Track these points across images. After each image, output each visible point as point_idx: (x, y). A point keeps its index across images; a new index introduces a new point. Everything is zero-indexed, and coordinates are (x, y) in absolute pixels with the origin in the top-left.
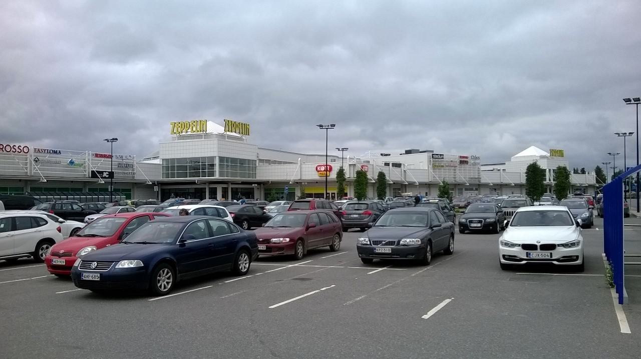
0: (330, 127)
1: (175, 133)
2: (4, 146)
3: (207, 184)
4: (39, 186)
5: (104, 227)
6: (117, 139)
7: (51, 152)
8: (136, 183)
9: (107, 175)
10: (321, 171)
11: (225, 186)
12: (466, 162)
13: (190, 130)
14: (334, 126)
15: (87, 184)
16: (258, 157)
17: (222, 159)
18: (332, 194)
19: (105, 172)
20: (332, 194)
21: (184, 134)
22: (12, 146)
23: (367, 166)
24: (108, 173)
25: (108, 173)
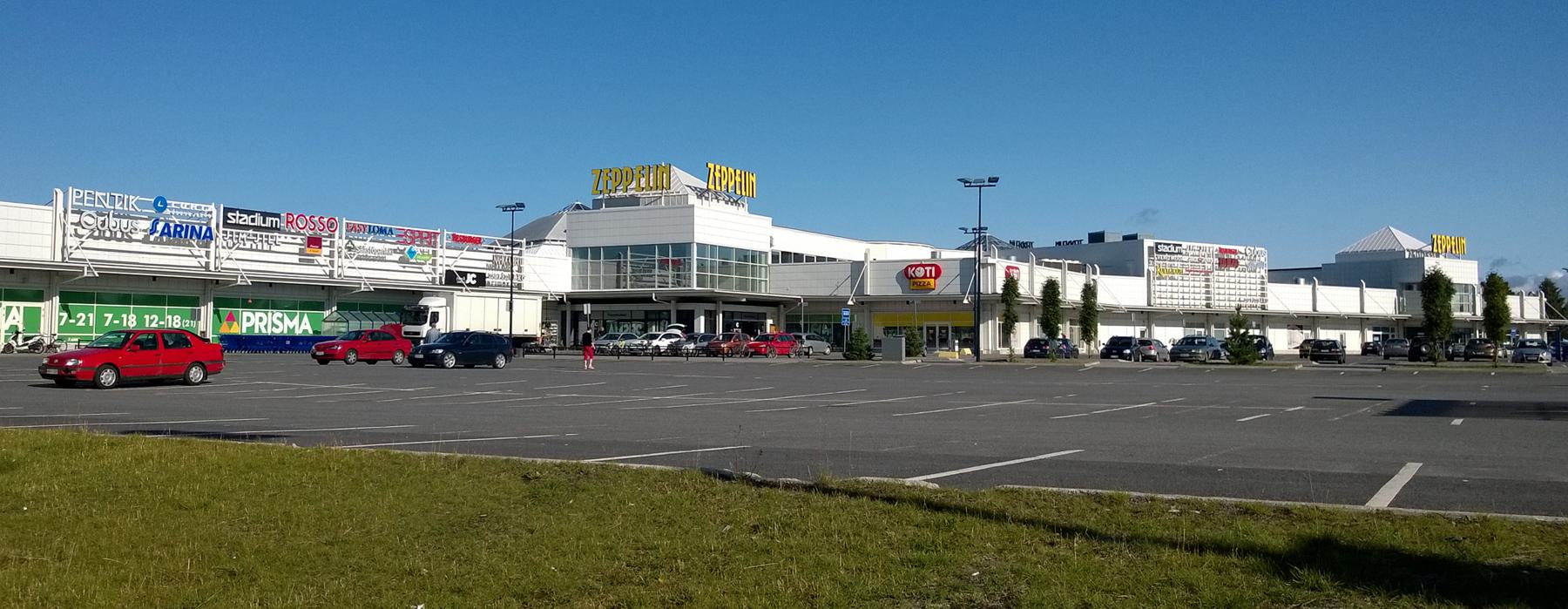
0: (986, 183)
1: (643, 188)
2: (295, 217)
3: (673, 302)
4: (353, 300)
5: (53, 382)
6: (522, 205)
7: (376, 229)
8: (154, 277)
9: (473, 279)
10: (916, 278)
11: (710, 307)
12: (1235, 263)
13: (633, 185)
14: (996, 180)
15: (335, 293)
16: (771, 245)
17: (782, 252)
18: (941, 328)
19: (471, 273)
20: (941, 328)
21: (620, 193)
22: (308, 218)
23: (1017, 268)
24: (475, 276)
25: (475, 276)
